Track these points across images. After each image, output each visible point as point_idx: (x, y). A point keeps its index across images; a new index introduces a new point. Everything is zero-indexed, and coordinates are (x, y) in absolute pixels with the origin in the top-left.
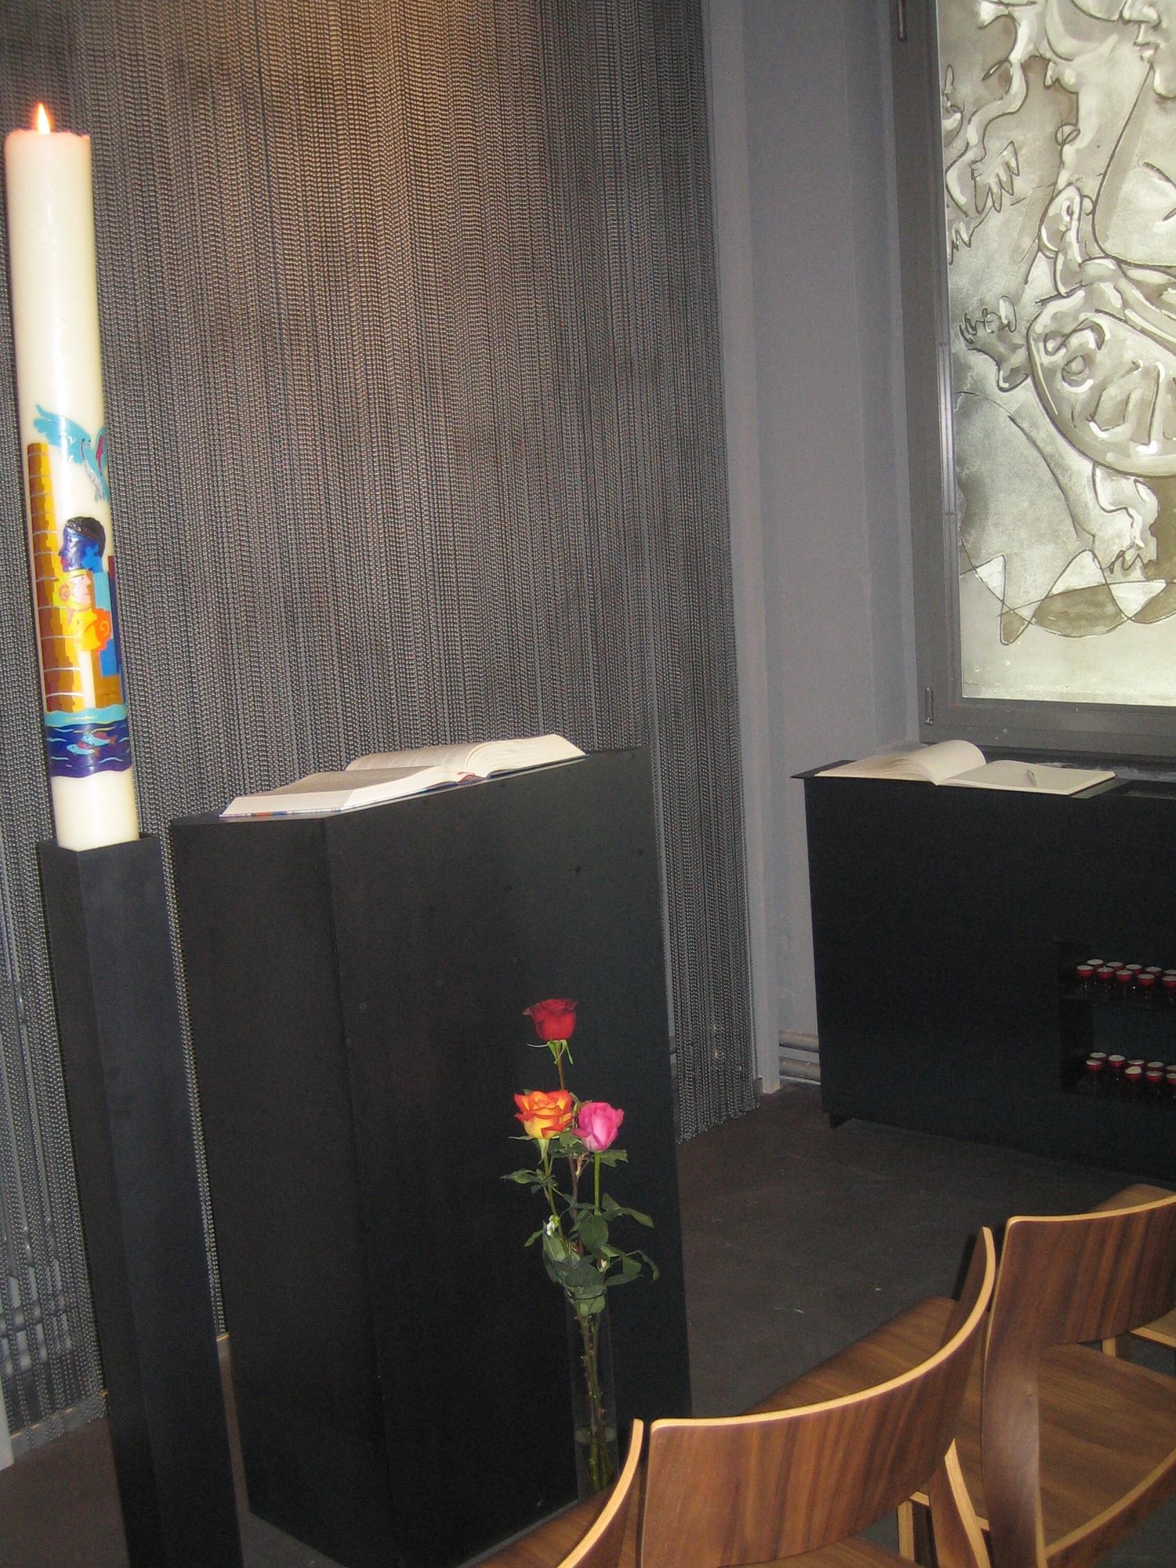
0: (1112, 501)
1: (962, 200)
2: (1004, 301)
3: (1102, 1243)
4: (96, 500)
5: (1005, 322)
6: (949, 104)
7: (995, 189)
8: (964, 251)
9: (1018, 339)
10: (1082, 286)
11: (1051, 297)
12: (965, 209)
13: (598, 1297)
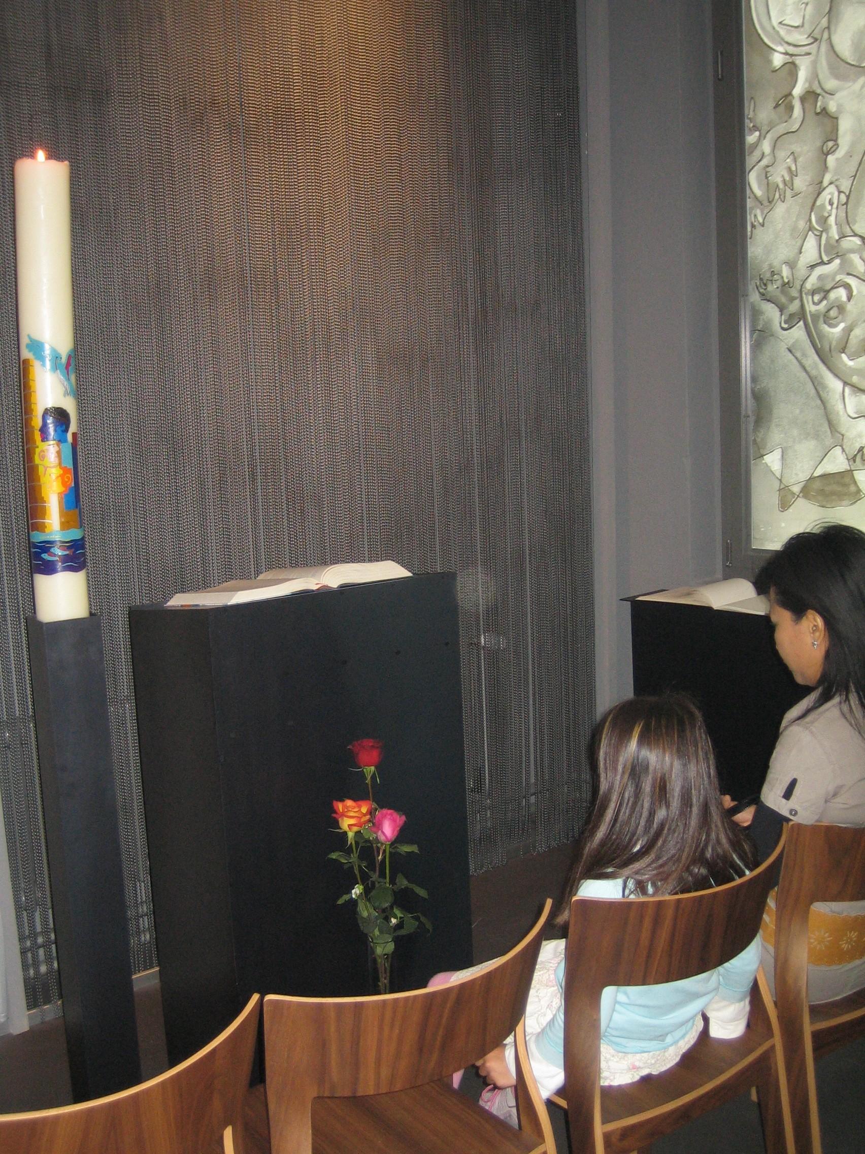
0: (856, 411)
1: (758, 192)
2: (786, 266)
3: (642, 917)
4: (65, 396)
5: (786, 280)
6: (752, 125)
7: (781, 186)
8: (759, 231)
9: (794, 293)
10: (838, 256)
11: (817, 264)
12: (760, 199)
13: (388, 942)
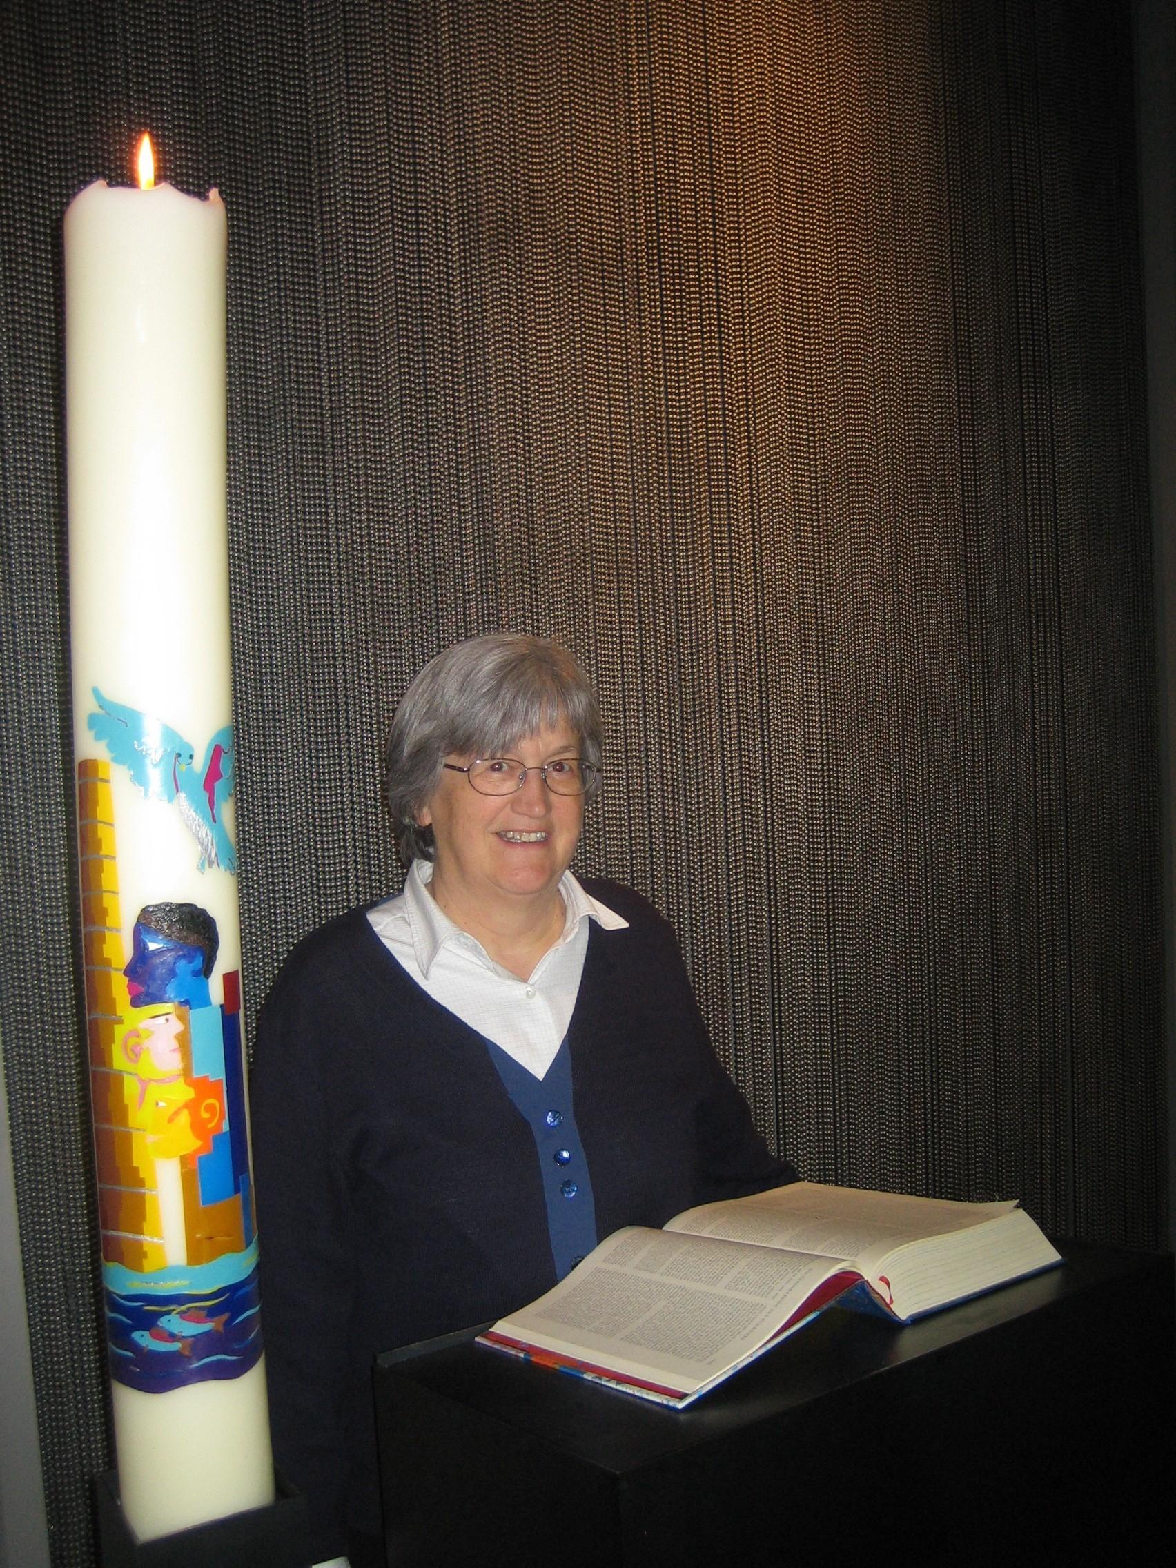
4: (201, 868)
